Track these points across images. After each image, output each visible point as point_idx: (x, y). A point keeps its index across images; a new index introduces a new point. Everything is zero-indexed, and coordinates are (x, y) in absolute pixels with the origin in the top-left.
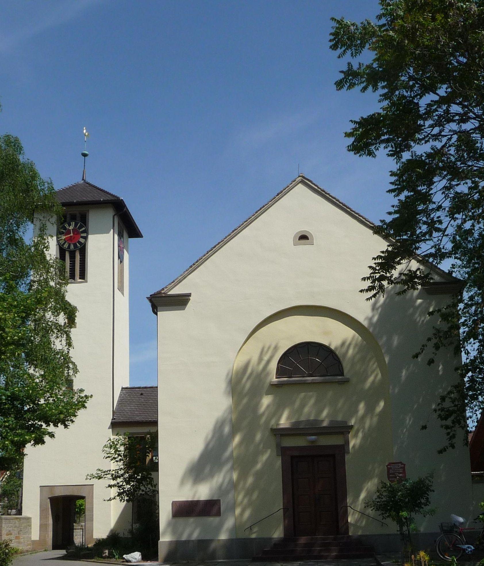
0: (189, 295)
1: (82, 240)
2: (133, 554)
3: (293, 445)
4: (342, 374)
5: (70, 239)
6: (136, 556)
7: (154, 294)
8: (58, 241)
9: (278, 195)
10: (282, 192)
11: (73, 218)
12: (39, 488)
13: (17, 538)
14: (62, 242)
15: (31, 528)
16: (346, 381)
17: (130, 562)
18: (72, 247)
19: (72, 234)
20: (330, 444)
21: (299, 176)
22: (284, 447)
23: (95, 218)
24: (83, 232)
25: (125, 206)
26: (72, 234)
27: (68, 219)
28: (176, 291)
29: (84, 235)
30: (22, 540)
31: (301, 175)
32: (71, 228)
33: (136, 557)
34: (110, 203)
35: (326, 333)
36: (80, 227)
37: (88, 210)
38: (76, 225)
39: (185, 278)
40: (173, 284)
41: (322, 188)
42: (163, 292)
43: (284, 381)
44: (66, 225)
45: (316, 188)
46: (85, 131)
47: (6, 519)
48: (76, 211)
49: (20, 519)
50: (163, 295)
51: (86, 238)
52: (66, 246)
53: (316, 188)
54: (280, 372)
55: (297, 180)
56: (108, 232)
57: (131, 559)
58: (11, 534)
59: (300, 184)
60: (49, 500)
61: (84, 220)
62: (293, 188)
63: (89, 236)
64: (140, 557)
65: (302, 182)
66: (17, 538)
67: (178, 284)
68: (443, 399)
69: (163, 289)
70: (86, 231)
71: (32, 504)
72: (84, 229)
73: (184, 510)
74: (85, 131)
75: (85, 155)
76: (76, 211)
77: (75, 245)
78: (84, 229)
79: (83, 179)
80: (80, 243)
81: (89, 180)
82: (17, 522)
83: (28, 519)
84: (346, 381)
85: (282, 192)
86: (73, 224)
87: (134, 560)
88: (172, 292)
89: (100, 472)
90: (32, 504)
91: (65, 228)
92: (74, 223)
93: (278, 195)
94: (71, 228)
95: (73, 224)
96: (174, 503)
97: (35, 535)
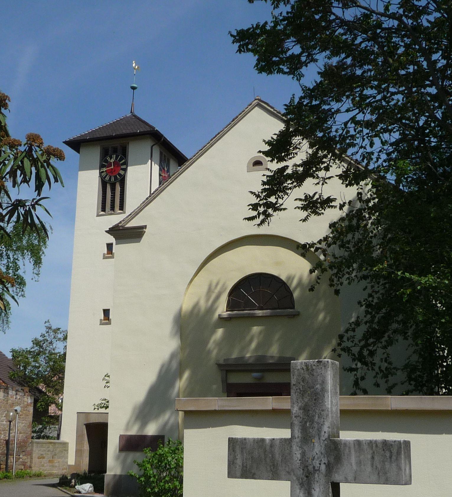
0: (145, 227)
1: (122, 172)
2: (84, 485)
3: (235, 382)
4: (293, 308)
5: (111, 171)
6: (87, 487)
7: (112, 228)
8: (101, 173)
9: (233, 120)
10: (237, 117)
11: (115, 151)
12: (76, 415)
13: (50, 461)
14: (104, 174)
15: (68, 453)
16: (297, 314)
17: (80, 492)
18: (113, 179)
19: (112, 167)
20: (240, 382)
21: (256, 99)
22: (230, 384)
23: (135, 149)
24: (123, 164)
25: (162, 136)
26: (112, 167)
27: (110, 152)
28: (133, 224)
29: (124, 167)
30: (57, 464)
31: (257, 98)
32: (112, 161)
33: (86, 488)
34: (147, 134)
35: (278, 264)
36: (120, 160)
37: (128, 143)
38: (116, 159)
39: (141, 210)
40: (130, 217)
41: (278, 110)
42: (120, 225)
43: (246, 314)
44: (108, 158)
45: (272, 110)
46: (134, 65)
47: (38, 443)
48: (116, 143)
49: (55, 443)
50: (121, 228)
51: (125, 170)
52: (107, 178)
53: (272, 110)
54: (231, 306)
55: (253, 103)
56: (146, 163)
57: (81, 490)
58: (44, 458)
59: (256, 107)
60: (84, 427)
61: (124, 153)
62: (249, 112)
63: (129, 168)
64: (92, 489)
65: (258, 105)
66: (50, 461)
67: (135, 217)
68: (341, 337)
69: (120, 222)
70: (126, 163)
71: (70, 431)
72: (124, 161)
73: (131, 444)
74: (134, 65)
75: (134, 88)
76: (116, 143)
77: (115, 177)
78: (124, 161)
79: (131, 112)
80: (120, 175)
81: (136, 113)
82: (51, 446)
83: (65, 445)
84: (297, 314)
85: (237, 117)
86: (114, 156)
87: (83, 492)
88: (128, 225)
89: (104, 402)
90: (70, 431)
91: (106, 161)
92: (115, 156)
93: (233, 120)
94: (112, 161)
95: (114, 156)
96: (121, 437)
97: (71, 460)
